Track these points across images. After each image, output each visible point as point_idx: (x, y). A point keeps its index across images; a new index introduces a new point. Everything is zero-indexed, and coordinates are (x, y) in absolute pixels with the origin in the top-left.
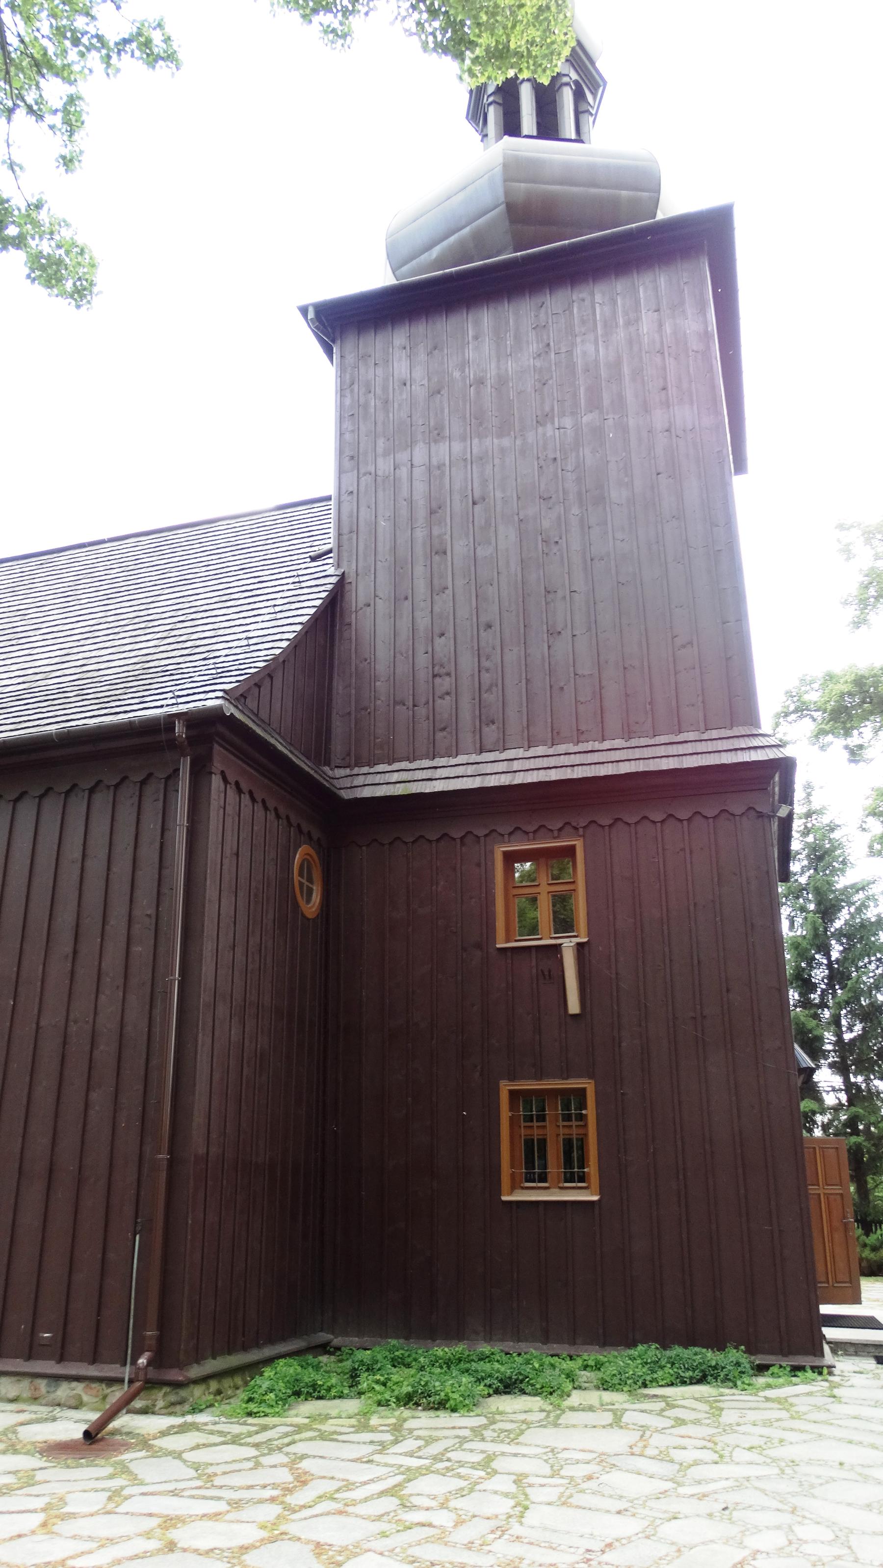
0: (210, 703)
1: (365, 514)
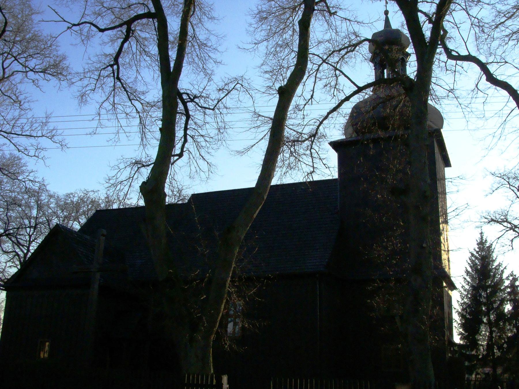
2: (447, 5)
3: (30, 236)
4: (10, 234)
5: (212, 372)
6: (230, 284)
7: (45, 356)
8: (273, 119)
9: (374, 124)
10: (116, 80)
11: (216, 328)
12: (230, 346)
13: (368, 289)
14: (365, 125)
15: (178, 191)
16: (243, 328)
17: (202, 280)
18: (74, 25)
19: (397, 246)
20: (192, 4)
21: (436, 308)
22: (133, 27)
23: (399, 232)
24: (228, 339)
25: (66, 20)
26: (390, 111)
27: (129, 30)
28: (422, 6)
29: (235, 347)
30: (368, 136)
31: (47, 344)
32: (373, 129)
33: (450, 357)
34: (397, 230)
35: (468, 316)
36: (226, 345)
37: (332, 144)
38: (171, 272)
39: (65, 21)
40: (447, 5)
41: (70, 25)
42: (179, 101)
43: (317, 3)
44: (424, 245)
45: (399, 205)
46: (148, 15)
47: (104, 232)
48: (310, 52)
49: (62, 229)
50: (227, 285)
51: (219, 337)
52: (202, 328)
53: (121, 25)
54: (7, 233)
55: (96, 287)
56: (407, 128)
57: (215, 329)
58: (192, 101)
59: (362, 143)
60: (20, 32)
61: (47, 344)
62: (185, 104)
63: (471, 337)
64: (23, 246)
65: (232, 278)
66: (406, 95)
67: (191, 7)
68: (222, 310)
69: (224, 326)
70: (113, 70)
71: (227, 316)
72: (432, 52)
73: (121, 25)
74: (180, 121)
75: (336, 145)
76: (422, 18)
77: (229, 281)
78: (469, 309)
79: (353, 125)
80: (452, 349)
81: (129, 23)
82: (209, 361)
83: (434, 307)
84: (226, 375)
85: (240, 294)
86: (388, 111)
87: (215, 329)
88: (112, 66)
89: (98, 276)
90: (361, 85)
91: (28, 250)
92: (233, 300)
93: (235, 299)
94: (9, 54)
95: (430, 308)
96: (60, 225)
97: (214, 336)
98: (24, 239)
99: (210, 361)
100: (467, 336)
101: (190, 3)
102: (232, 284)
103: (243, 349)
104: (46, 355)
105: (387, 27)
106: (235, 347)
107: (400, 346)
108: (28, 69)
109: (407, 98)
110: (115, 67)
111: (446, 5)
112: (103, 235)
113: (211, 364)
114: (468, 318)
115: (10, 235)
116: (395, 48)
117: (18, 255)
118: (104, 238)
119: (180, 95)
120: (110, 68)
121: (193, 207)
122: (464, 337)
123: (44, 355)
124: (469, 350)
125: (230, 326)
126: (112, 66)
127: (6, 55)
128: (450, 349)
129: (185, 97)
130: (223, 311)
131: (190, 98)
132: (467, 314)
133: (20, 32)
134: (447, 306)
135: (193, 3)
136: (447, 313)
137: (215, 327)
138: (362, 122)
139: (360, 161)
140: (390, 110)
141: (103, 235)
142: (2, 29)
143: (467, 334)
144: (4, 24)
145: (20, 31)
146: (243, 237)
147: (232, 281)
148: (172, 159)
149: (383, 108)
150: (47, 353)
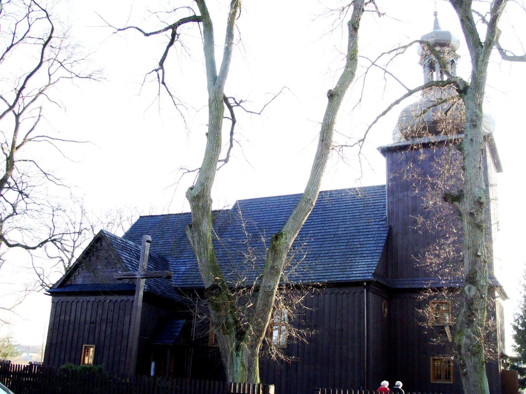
0: (369, 277)
1: (395, 209)
2: (504, 3)
3: (75, 242)
4: (55, 240)
5: (258, 381)
6: (277, 292)
7: (90, 362)
8: (322, 123)
9: (424, 128)
10: (161, 84)
11: (263, 337)
12: (277, 355)
13: (419, 298)
14: (415, 129)
15: (80, 234)
16: (290, 338)
17: (249, 288)
18: (120, 30)
19: (450, 254)
20: (238, 6)
21: (490, 319)
22: (178, 31)
23: (451, 239)
24: (274, 349)
25: (111, 25)
26: (441, 115)
27: (174, 35)
28: (474, 6)
29: (282, 356)
30: (418, 140)
31: (92, 349)
32: (423, 134)
33: (503, 369)
34: (449, 237)
35: (520, 328)
36: (273, 354)
37: (380, 149)
38: (217, 279)
39: (110, 26)
40: (504, 3)
41: (116, 30)
42: (225, 104)
43: (366, 4)
44: (479, 254)
45: (452, 212)
46: (195, 19)
47: (150, 238)
48: (225, 116)
49: (106, 235)
50: (275, 293)
51: (266, 346)
52: (249, 337)
53: (166, 29)
54: (52, 238)
55: (141, 293)
56: (459, 133)
57: (262, 338)
58: (238, 105)
59: (412, 148)
60: (66, 38)
61: (92, 349)
62: (230, 107)
63: (523, 350)
64: (68, 251)
65: (280, 285)
66: (461, 96)
67: (237, 10)
68: (269, 318)
69: (270, 335)
70: (158, 75)
71: (271, 325)
72: (487, 54)
73: (166, 29)
74: (226, 125)
75: (387, 151)
76: (476, 18)
77: (276, 289)
78: (521, 320)
79: (401, 131)
80: (504, 361)
81: (174, 27)
82: (256, 371)
83: (489, 318)
84: (273, 385)
85: (288, 302)
86: (439, 114)
87: (262, 338)
88: (156, 70)
89: (143, 282)
90: (412, 88)
91: (73, 256)
92: (281, 309)
93: (283, 307)
94: (55, 60)
95: (485, 320)
96: (104, 231)
97: (261, 345)
98: (68, 244)
99: (257, 370)
100: (519, 348)
101: (236, 6)
102: (279, 292)
103: (290, 359)
104: (91, 361)
105: (436, 29)
106: (282, 356)
107: (452, 358)
108: (73, 75)
109: (461, 101)
110: (160, 72)
111: (503, 2)
112: (148, 241)
113: (257, 374)
114: (520, 329)
115: (56, 241)
116: (446, 49)
117: (63, 260)
118: (149, 244)
119: (226, 99)
120: (155, 73)
121: (240, 213)
122: (516, 349)
123: (89, 360)
124: (521, 363)
125: (275, 333)
126: (156, 70)
127: (52, 61)
128: (503, 361)
129: (231, 101)
130: (271, 319)
131: (236, 103)
132: (519, 326)
133: (66, 38)
134: (499, 316)
135: (239, 5)
136: (499, 324)
137: (261, 336)
138: (412, 127)
139: (410, 167)
140: (441, 113)
141: (148, 241)
142: (49, 36)
143: (519, 346)
144: (51, 31)
145: (65, 37)
146: (291, 244)
147: (280, 289)
148: (219, 164)
149: (433, 111)
150: (92, 359)
